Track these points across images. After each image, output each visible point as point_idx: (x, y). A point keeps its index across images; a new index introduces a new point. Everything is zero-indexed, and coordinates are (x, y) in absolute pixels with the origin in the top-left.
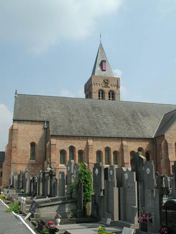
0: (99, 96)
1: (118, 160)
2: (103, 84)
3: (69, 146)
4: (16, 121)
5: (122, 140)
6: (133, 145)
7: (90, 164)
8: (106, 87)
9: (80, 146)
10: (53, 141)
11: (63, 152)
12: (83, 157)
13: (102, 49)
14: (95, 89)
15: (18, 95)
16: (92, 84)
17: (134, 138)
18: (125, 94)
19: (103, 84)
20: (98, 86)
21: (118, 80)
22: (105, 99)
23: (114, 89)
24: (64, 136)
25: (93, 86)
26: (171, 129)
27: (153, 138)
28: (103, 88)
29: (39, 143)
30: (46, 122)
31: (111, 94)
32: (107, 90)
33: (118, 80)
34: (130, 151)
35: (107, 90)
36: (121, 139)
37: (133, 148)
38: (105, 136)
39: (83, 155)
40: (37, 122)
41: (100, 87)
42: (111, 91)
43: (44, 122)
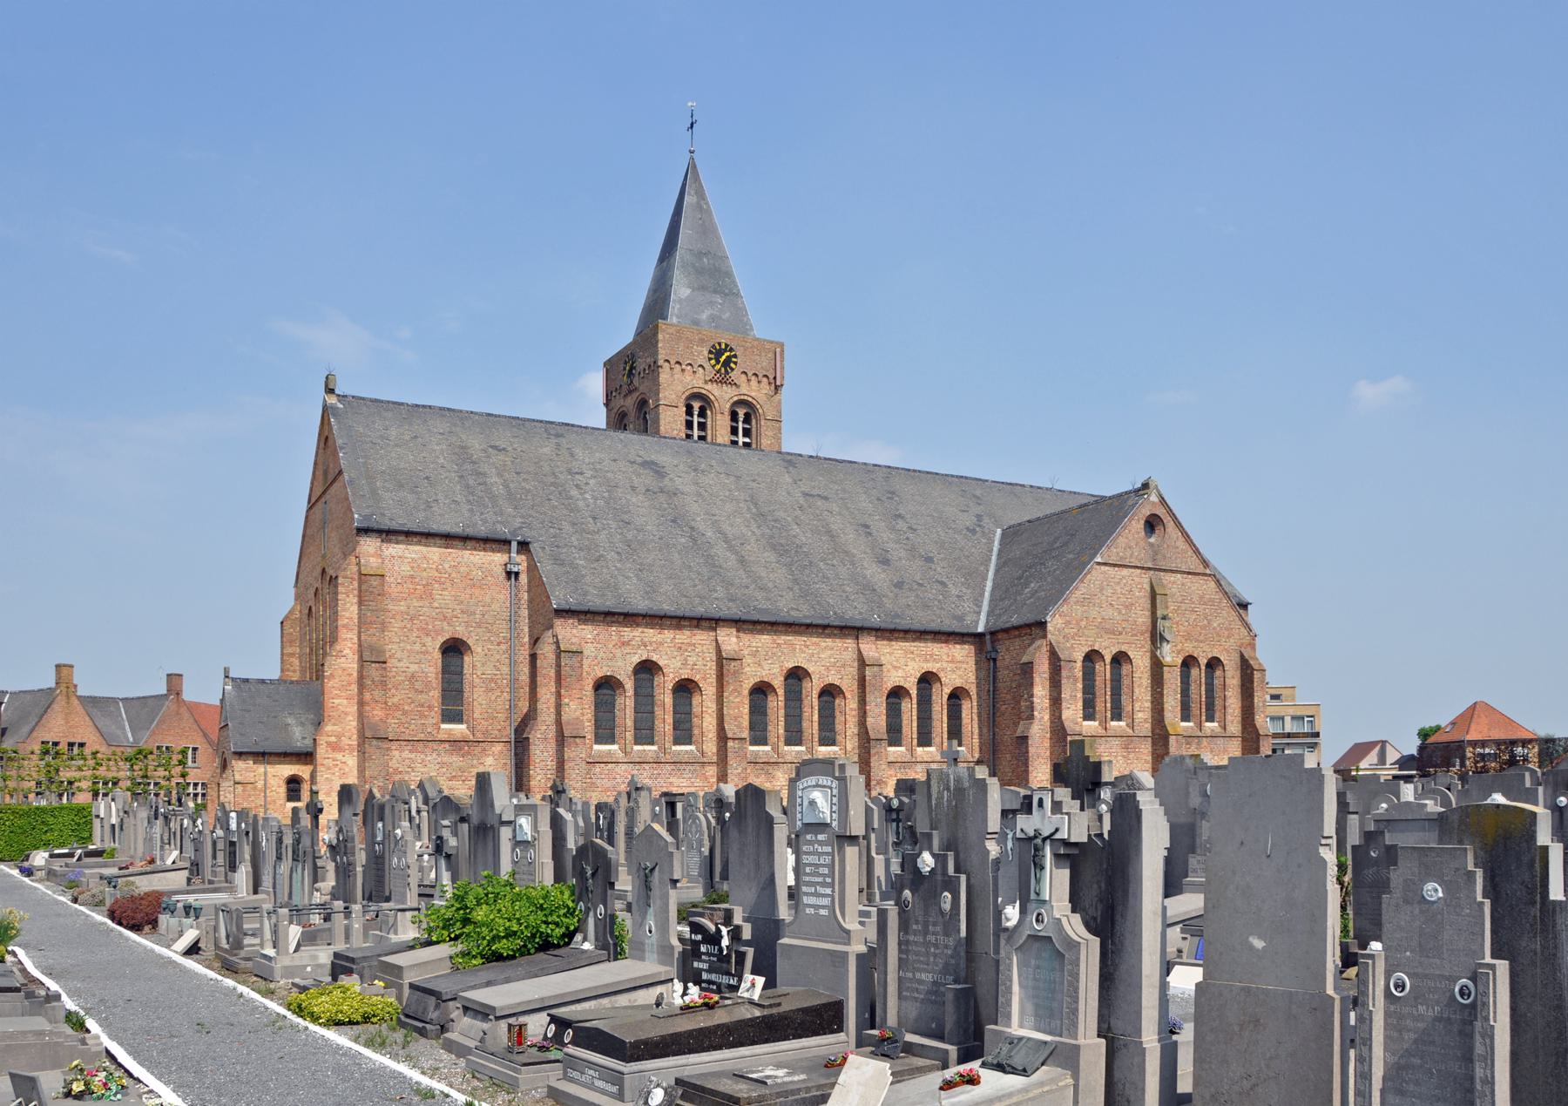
0: (689, 425)
1: (839, 727)
2: (707, 365)
3: (636, 659)
4: (438, 541)
5: (715, 630)
6: (902, 661)
7: (730, 744)
8: (723, 378)
9: (685, 664)
10: (570, 632)
11: (606, 686)
12: (696, 710)
13: (695, 166)
14: (673, 387)
15: (342, 398)
16: (661, 362)
17: (906, 632)
18: (799, 431)
19: (707, 365)
20: (688, 377)
21: (776, 351)
22: (657, 432)
23: (756, 391)
24: (613, 614)
25: (664, 376)
26: (1073, 599)
27: (981, 635)
28: (709, 386)
29: (972, 678)
30: (514, 545)
31: (741, 417)
32: (724, 396)
33: (776, 351)
34: (890, 685)
35: (724, 396)
36: (853, 630)
37: (900, 673)
38: (892, 626)
39: (696, 700)
40: (473, 543)
41: (696, 381)
42: (741, 403)
43: (507, 542)
